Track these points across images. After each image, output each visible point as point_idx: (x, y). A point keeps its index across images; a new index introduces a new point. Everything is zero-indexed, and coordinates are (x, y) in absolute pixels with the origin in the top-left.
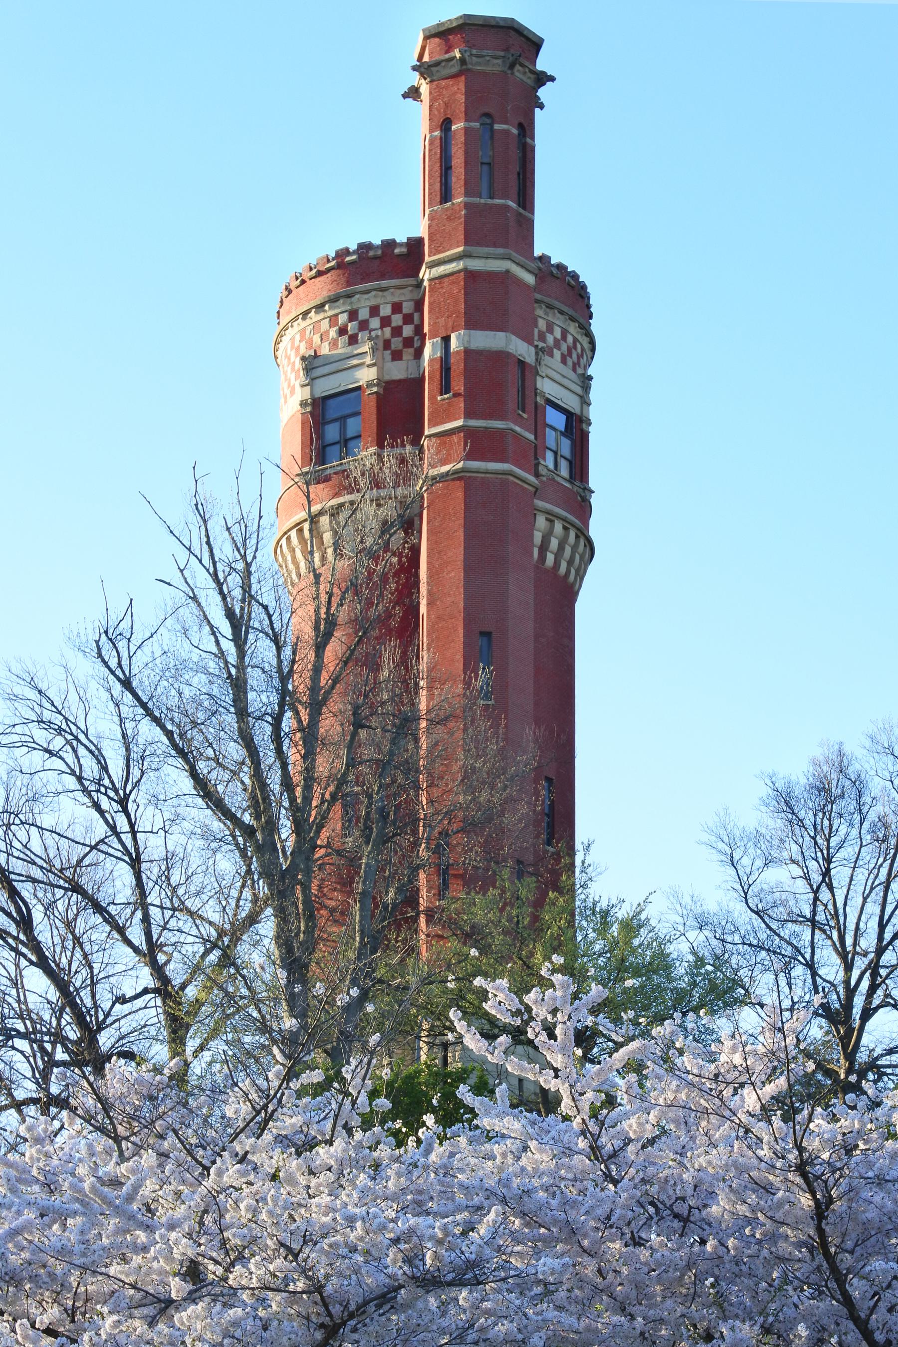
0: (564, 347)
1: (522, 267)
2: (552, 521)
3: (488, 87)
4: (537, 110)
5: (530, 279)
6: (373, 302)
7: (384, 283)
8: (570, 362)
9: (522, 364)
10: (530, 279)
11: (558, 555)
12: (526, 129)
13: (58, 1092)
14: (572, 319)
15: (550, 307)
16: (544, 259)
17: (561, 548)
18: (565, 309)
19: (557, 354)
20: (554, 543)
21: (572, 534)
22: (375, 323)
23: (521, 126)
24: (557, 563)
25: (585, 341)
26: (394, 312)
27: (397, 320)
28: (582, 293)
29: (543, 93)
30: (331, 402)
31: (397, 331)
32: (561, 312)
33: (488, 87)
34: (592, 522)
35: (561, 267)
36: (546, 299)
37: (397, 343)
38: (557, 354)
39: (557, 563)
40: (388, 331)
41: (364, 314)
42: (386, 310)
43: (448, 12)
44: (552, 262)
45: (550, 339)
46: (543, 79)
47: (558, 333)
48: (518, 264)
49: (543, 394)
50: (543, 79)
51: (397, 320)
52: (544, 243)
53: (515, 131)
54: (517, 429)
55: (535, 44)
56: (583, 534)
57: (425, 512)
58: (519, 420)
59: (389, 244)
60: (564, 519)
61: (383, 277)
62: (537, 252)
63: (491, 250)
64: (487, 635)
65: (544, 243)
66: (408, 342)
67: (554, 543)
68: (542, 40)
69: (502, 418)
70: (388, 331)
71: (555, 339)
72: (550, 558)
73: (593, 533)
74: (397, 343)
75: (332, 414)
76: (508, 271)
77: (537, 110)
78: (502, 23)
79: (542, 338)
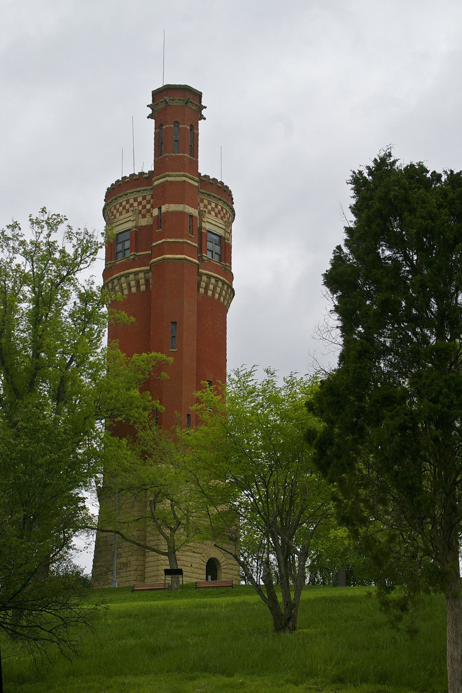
0: (216, 210)
1: (192, 179)
2: (210, 278)
3: (176, 112)
4: (455, 173)
5: (196, 184)
6: (135, 196)
7: (139, 189)
8: (219, 216)
9: (191, 216)
10: (196, 184)
11: (220, 294)
12: (194, 128)
14: (220, 199)
15: (209, 195)
17: (215, 288)
18: (215, 195)
21: (226, 287)
22: (136, 204)
24: (219, 298)
26: (143, 200)
27: (144, 202)
28: (226, 190)
29: (150, 111)
30: (120, 236)
31: (144, 207)
32: (214, 197)
34: (234, 282)
36: (208, 192)
37: (144, 211)
38: (213, 213)
39: (219, 298)
40: (140, 207)
41: (131, 201)
42: (140, 199)
44: (211, 178)
47: (213, 205)
48: (190, 178)
49: (205, 229)
51: (144, 202)
52: (203, 170)
53: (189, 128)
54: (189, 242)
56: (230, 287)
58: (190, 238)
60: (216, 277)
61: (139, 186)
63: (178, 173)
64: (174, 323)
65: (203, 170)
67: (211, 287)
68: (202, 93)
69: (182, 238)
71: (212, 207)
72: (210, 293)
73: (234, 287)
74: (144, 211)
75: (120, 240)
76: (184, 181)
77: (455, 173)
78: (182, 87)
79: (205, 206)
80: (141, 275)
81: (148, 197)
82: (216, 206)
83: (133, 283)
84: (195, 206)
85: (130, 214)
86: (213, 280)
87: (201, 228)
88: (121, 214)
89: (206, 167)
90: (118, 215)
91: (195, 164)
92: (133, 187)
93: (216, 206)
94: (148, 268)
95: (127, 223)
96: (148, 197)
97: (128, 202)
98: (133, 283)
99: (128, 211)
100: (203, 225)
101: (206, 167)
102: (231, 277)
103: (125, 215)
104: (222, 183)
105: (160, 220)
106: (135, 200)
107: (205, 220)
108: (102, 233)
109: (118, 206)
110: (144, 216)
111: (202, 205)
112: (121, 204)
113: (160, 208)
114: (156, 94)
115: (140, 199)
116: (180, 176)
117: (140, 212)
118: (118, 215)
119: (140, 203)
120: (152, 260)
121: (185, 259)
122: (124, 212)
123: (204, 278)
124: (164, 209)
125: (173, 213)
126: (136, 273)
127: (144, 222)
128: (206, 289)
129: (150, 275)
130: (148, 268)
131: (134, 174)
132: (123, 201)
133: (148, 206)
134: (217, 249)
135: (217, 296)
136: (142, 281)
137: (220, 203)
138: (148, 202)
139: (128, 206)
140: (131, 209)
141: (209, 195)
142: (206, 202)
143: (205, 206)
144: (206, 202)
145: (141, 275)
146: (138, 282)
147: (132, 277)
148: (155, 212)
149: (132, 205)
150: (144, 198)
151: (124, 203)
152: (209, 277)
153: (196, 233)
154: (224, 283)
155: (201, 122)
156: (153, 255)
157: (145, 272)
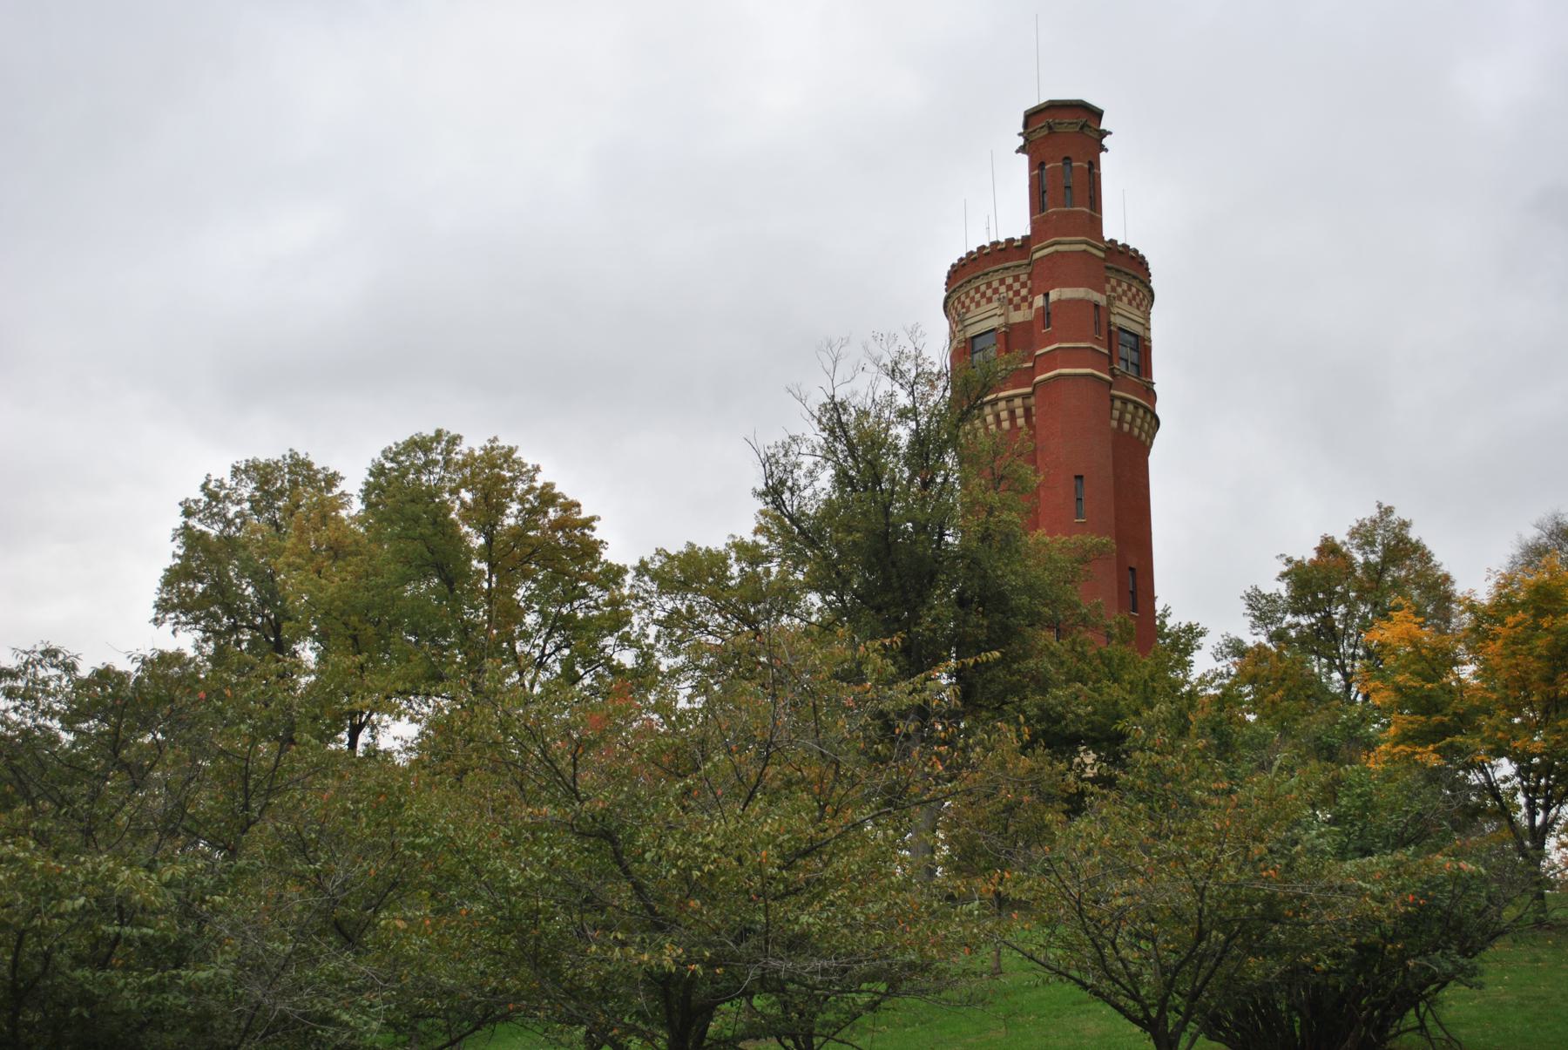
3: (1064, 142)
5: (1102, 255)
9: (1097, 306)
10: (1102, 255)
11: (1131, 424)
12: (1094, 165)
13: (1448, 1015)
15: (1118, 271)
16: (1112, 242)
17: (1133, 418)
19: (1125, 299)
20: (1128, 417)
22: (1003, 289)
23: (1090, 163)
24: (1131, 429)
25: (1146, 291)
27: (1017, 286)
29: (1021, 141)
31: (1017, 293)
33: (1064, 142)
35: (1125, 246)
37: (1016, 300)
38: (1125, 299)
39: (1131, 429)
40: (1011, 294)
41: (995, 284)
42: (1009, 281)
43: (1033, 102)
45: (1119, 290)
46: (1105, 134)
47: (1125, 286)
50: (1105, 134)
51: (1017, 286)
55: (1098, 114)
57: (1002, 394)
59: (1010, 241)
60: (1134, 402)
62: (1107, 238)
65: (1108, 233)
66: (1024, 299)
67: (1128, 417)
70: (1011, 294)
72: (1126, 427)
73: (1158, 412)
75: (978, 347)
79: (1114, 289)
80: (1018, 402)
81: (1023, 278)
82: (1130, 287)
83: (1004, 415)
84: (1102, 291)
85: (995, 304)
86: (1130, 407)
87: (1109, 324)
88: (978, 305)
89: (1113, 229)
90: (973, 306)
91: (1096, 223)
92: (996, 262)
93: (1130, 287)
94: (1029, 390)
95: (988, 317)
96: (1023, 278)
97: (989, 285)
98: (1004, 415)
99: (990, 300)
100: (1113, 319)
101: (1113, 229)
102: (1151, 395)
103: (985, 307)
104: (1136, 251)
105: (1046, 315)
106: (1002, 282)
107: (1115, 310)
108: (496, 439)
109: (972, 293)
110: (1017, 308)
111: (1108, 287)
112: (977, 290)
113: (1047, 295)
114: (1031, 117)
115: (1009, 281)
116: (1070, 243)
117: (1010, 301)
118: (973, 306)
119: (1009, 288)
120: (1038, 378)
121: (1060, 375)
122: (984, 301)
123: (1118, 404)
124: (1054, 295)
125: (1069, 301)
126: (1009, 399)
127: (1017, 317)
128: (1121, 420)
129: (1032, 400)
130: (1029, 390)
131: (998, 243)
132: (981, 283)
133: (1024, 292)
134: (1133, 356)
135: (1136, 431)
136: (1019, 412)
137: (1135, 283)
138: (1024, 285)
139: (978, 296)
140: (996, 297)
141: (1118, 271)
142: (1113, 282)
143: (1114, 289)
144: (1113, 282)
145: (1018, 402)
146: (1012, 413)
147: (1002, 404)
148: (1039, 301)
149: (996, 291)
150: (1016, 279)
151: (983, 288)
152: (1125, 401)
153: (1104, 332)
154: (1137, 405)
155: (1103, 155)
156: (1037, 369)
157: (1025, 396)
